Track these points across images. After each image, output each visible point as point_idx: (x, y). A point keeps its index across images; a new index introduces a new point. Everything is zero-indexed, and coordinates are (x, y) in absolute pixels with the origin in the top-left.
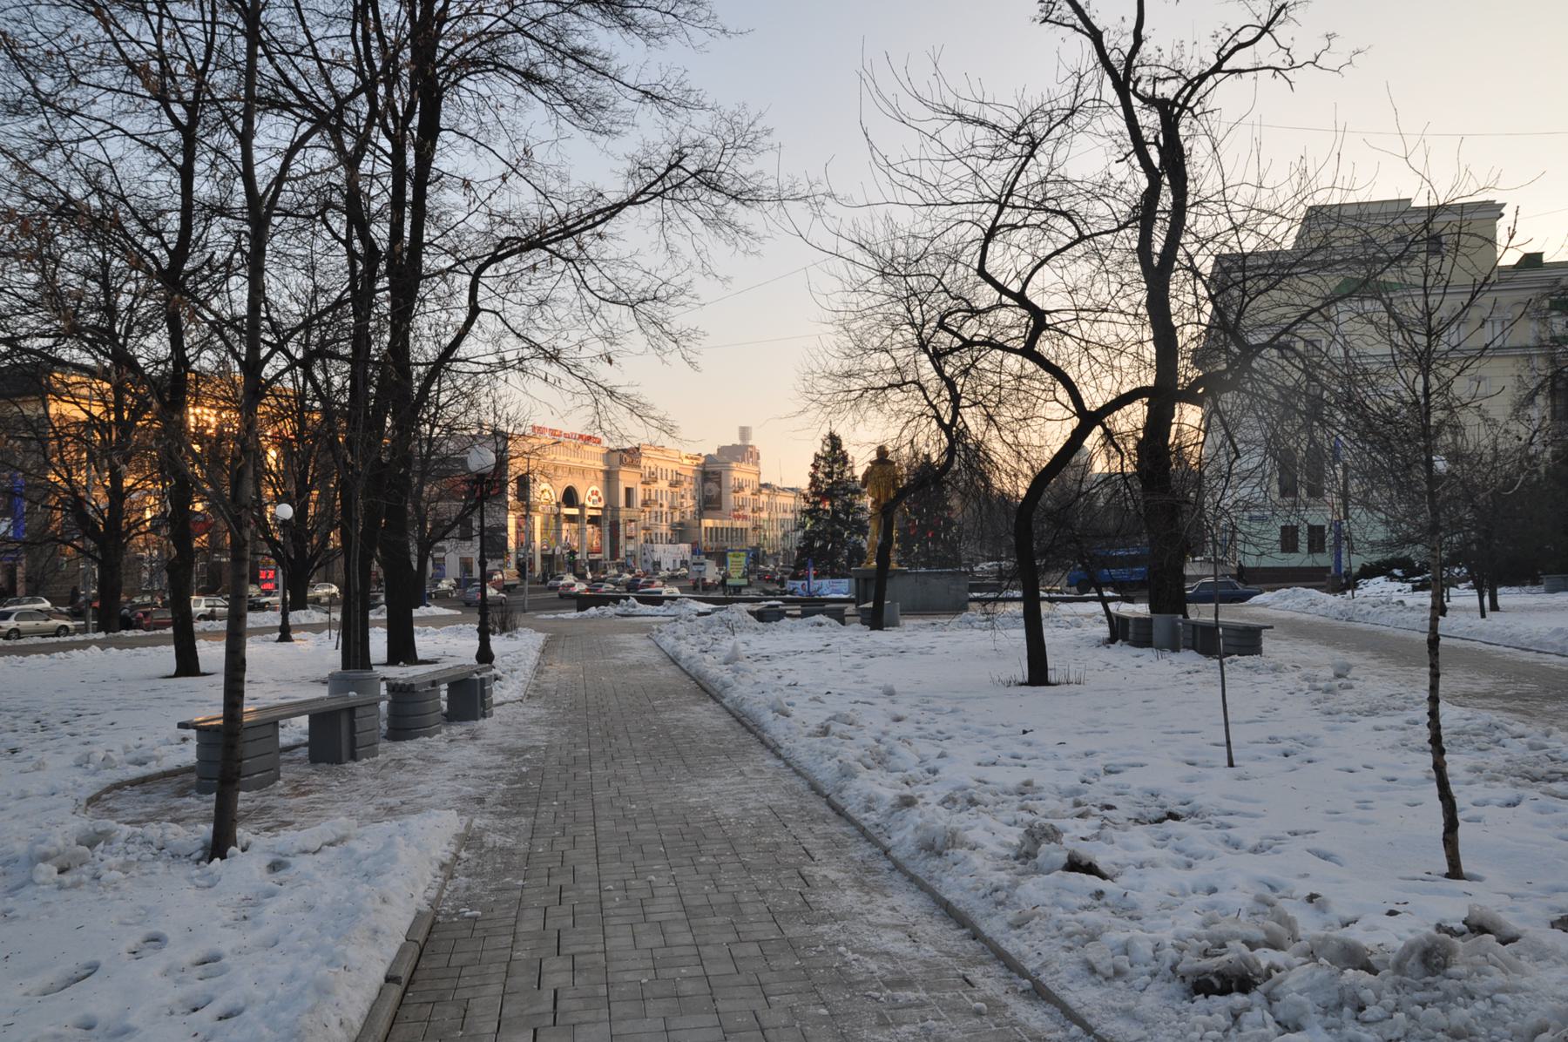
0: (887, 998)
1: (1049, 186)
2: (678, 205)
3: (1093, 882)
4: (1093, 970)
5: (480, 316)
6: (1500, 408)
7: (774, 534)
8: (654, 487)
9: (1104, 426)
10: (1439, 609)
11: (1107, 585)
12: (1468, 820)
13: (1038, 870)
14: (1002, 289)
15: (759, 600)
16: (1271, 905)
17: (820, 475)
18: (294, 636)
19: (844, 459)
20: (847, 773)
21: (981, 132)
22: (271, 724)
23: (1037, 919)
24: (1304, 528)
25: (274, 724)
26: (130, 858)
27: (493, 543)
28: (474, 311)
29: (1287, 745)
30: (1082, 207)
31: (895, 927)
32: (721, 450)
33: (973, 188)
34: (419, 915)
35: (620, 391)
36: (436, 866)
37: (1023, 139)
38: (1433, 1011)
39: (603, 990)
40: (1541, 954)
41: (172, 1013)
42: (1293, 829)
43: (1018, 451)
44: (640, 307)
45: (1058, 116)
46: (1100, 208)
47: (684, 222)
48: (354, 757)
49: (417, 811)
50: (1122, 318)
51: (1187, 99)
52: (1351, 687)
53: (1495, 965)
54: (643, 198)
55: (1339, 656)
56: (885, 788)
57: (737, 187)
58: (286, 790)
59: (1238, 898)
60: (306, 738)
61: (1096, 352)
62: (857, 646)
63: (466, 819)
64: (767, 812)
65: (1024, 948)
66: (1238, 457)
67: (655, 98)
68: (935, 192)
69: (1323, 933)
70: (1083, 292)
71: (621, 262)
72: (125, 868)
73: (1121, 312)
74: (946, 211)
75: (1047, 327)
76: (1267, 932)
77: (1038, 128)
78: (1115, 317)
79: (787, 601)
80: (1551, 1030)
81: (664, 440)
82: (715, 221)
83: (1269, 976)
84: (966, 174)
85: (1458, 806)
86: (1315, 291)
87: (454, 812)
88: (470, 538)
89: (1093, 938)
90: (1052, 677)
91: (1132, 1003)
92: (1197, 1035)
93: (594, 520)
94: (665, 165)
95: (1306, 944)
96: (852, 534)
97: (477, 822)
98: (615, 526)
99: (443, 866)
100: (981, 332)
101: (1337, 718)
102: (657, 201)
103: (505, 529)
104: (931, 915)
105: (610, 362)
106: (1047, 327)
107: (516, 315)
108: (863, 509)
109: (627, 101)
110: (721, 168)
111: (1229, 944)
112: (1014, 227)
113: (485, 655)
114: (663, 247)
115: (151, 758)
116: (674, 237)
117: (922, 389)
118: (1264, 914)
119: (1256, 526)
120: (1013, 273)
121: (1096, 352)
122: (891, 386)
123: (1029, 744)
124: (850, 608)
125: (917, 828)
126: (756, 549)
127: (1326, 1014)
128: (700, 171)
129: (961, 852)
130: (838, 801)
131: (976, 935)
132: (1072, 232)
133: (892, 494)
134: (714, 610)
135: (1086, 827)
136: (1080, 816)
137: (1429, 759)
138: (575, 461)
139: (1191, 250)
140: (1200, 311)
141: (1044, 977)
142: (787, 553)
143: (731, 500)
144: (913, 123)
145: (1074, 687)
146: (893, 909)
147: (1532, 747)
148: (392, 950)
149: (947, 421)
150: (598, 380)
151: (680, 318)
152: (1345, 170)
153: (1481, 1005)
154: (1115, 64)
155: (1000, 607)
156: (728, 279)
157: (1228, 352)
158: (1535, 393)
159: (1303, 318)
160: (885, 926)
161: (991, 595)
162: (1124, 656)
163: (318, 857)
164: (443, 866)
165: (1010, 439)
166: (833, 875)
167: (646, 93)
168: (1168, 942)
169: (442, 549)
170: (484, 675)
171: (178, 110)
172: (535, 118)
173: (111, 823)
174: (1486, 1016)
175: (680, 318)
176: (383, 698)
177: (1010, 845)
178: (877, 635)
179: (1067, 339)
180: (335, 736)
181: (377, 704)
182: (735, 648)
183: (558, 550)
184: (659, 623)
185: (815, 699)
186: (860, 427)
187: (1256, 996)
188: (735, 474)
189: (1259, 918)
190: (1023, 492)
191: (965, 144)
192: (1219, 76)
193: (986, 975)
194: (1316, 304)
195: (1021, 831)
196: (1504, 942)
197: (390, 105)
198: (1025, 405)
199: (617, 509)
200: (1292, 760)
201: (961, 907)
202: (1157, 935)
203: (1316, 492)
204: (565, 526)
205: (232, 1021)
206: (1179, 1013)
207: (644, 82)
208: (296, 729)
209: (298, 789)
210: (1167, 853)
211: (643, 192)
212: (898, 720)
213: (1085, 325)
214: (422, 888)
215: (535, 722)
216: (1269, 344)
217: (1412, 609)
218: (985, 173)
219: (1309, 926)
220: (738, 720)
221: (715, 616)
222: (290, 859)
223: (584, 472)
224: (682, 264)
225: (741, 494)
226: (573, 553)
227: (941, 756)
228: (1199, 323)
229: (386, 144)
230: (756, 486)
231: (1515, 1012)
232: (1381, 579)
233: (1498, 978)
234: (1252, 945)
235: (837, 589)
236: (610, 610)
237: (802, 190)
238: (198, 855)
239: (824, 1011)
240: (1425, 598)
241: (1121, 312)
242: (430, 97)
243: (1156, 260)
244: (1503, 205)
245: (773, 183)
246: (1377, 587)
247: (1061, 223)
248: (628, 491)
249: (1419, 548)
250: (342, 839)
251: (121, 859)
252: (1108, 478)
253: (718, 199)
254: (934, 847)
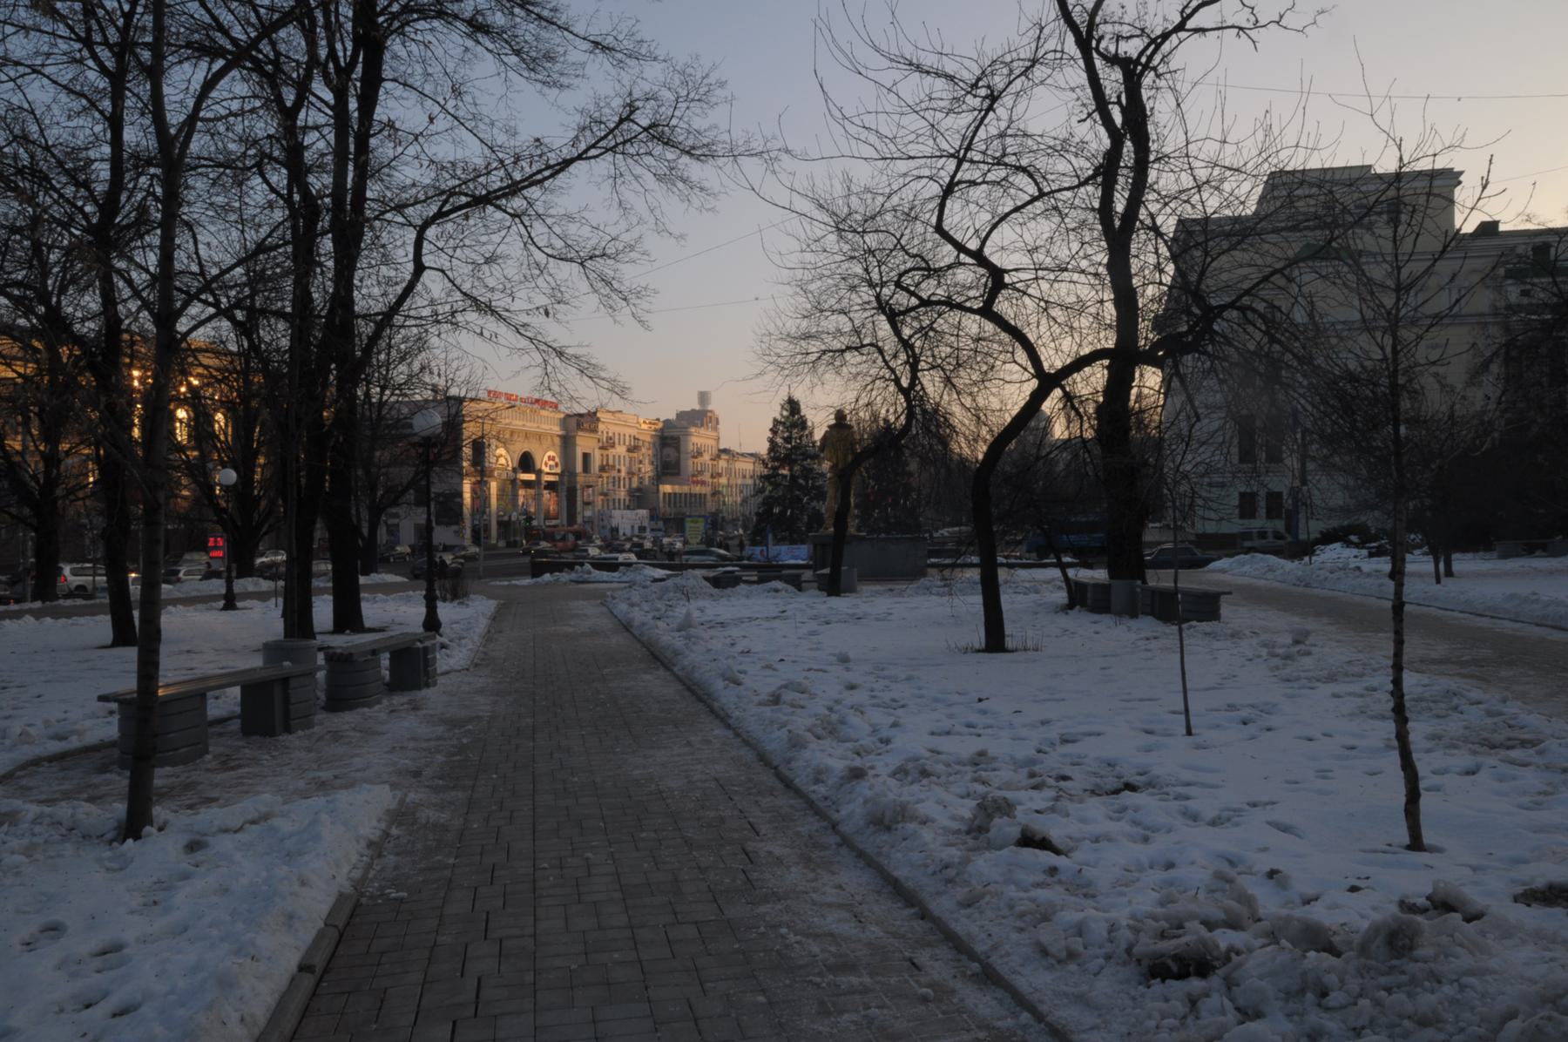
0: (829, 984)
1: (1009, 141)
2: (629, 161)
3: (1047, 858)
4: (1044, 952)
5: (426, 273)
6: (1456, 374)
7: (733, 499)
8: (612, 452)
9: (1063, 388)
10: (1397, 574)
11: (1066, 551)
12: (1428, 790)
13: (991, 846)
14: (960, 248)
15: (715, 566)
16: (1230, 881)
17: (779, 440)
18: (239, 604)
19: (802, 424)
20: (796, 744)
21: (940, 83)
22: (196, 696)
23: (988, 898)
24: (1262, 493)
25: (202, 696)
26: (35, 840)
27: (449, 509)
28: (419, 268)
29: (1244, 713)
30: (1042, 163)
31: (840, 906)
32: (681, 415)
33: (931, 142)
34: (342, 897)
35: (570, 351)
36: (363, 843)
37: (983, 92)
38: (1400, 996)
39: (529, 978)
40: (1507, 932)
41: (62, 1011)
43: (978, 415)
44: (588, 264)
45: (1018, 67)
46: (1062, 166)
47: (636, 178)
48: (288, 730)
49: (350, 785)
50: (1082, 278)
51: (1150, 58)
52: (1309, 654)
53: (1461, 945)
54: (593, 152)
55: (1297, 621)
56: (835, 759)
57: (690, 142)
58: (214, 764)
59: (1196, 874)
60: (238, 710)
61: (1056, 312)
62: (814, 612)
63: (399, 794)
64: (713, 785)
65: (974, 929)
66: (1198, 419)
67: (606, 49)
68: (891, 146)
69: (1284, 912)
70: (1042, 250)
71: (570, 218)
72: (28, 851)
73: (1083, 272)
74: (902, 166)
75: (1006, 286)
76: (1226, 911)
77: (999, 81)
78: (1076, 276)
79: (744, 567)
80: (1521, 1017)
81: (616, 403)
82: (669, 177)
83: (1229, 959)
84: (925, 127)
85: (1420, 774)
86: (1278, 253)
87: (387, 787)
89: (1046, 918)
90: (1009, 643)
91: (1085, 988)
92: (1152, 1023)
93: (551, 486)
94: (616, 119)
95: (1266, 925)
96: (811, 499)
97: (412, 796)
99: (371, 844)
100: (939, 291)
101: (1295, 685)
102: (609, 156)
103: (460, 495)
104: (879, 893)
105: (547, 314)
106: (1006, 286)
107: (461, 271)
108: (823, 475)
109: (577, 53)
110: (674, 122)
111: (1187, 925)
112: (973, 183)
113: (432, 623)
114: (615, 204)
115: (73, 732)
116: (627, 195)
117: (881, 351)
118: (1224, 891)
119: (1216, 492)
120: (972, 230)
121: (1056, 312)
122: (849, 348)
123: (984, 712)
124: (807, 575)
125: (866, 802)
126: (715, 515)
127: (1287, 1000)
128: (651, 127)
129: (911, 826)
130: (787, 773)
131: (924, 915)
132: (1032, 190)
133: (850, 458)
134: (669, 576)
135: (1040, 799)
136: (1035, 787)
137: (1390, 727)
138: (531, 426)
139: (1154, 207)
140: (1161, 271)
141: (994, 960)
142: (746, 519)
143: (690, 465)
144: (871, 74)
145: (1031, 654)
146: (840, 887)
147: (1490, 714)
148: (307, 934)
149: (905, 383)
150: (549, 340)
151: (629, 274)
152: (1310, 126)
153: (1448, 990)
154: (1078, 20)
155: (958, 573)
156: (682, 236)
157: (1190, 313)
158: (1490, 361)
159: (1266, 279)
160: (830, 905)
161: (948, 561)
162: (1083, 624)
163: (239, 836)
164: (371, 844)
165: (968, 402)
166: (778, 851)
167: (596, 44)
168: (1124, 923)
169: (396, 516)
170: (427, 644)
171: (104, 54)
172: (486, 74)
173: (17, 803)
174: (1453, 1001)
175: (629, 274)
176: (320, 668)
177: (962, 819)
178: (835, 602)
179: (1026, 299)
180: (269, 707)
181: (311, 674)
182: (688, 615)
183: (514, 516)
184: (613, 590)
185: (768, 667)
186: (818, 389)
187: (1215, 981)
188: (694, 439)
189: (1218, 895)
190: (981, 457)
191: (922, 96)
192: (1182, 35)
193: (934, 958)
194: (1279, 265)
195: (974, 803)
196: (1469, 919)
197: (332, 54)
198: (984, 368)
199: (573, 475)
200: (1252, 729)
201: (910, 884)
202: (1113, 914)
203: (1275, 458)
204: (521, 492)
205: (126, 1018)
206: (1134, 999)
207: (595, 31)
208: (228, 701)
209: (226, 764)
210: (1124, 826)
211: (593, 146)
212: (852, 687)
213: (1045, 285)
214: (345, 869)
215: (480, 691)
216: (1232, 305)
217: (1369, 575)
218: (943, 126)
219: (1269, 903)
220: (689, 689)
221: (670, 583)
222: (208, 839)
223: (540, 437)
224: (634, 220)
225: (700, 460)
226: (529, 519)
227: (895, 725)
228: (1161, 283)
229: (328, 96)
230: (715, 452)
231: (1483, 996)
232: (1337, 545)
233: (1465, 960)
234: (1210, 925)
235: (795, 555)
236: (565, 576)
237: (757, 145)
238: (110, 836)
239: (761, 999)
240: (1384, 564)
241: (1083, 272)
242: (371, 44)
243: (1117, 223)
244: (1461, 173)
245: (726, 137)
246: (1334, 553)
247: (1022, 180)
248: (586, 456)
249: (1377, 513)
250: (266, 817)
251: (25, 841)
252: (1066, 444)
253: (670, 154)
254: (886, 820)
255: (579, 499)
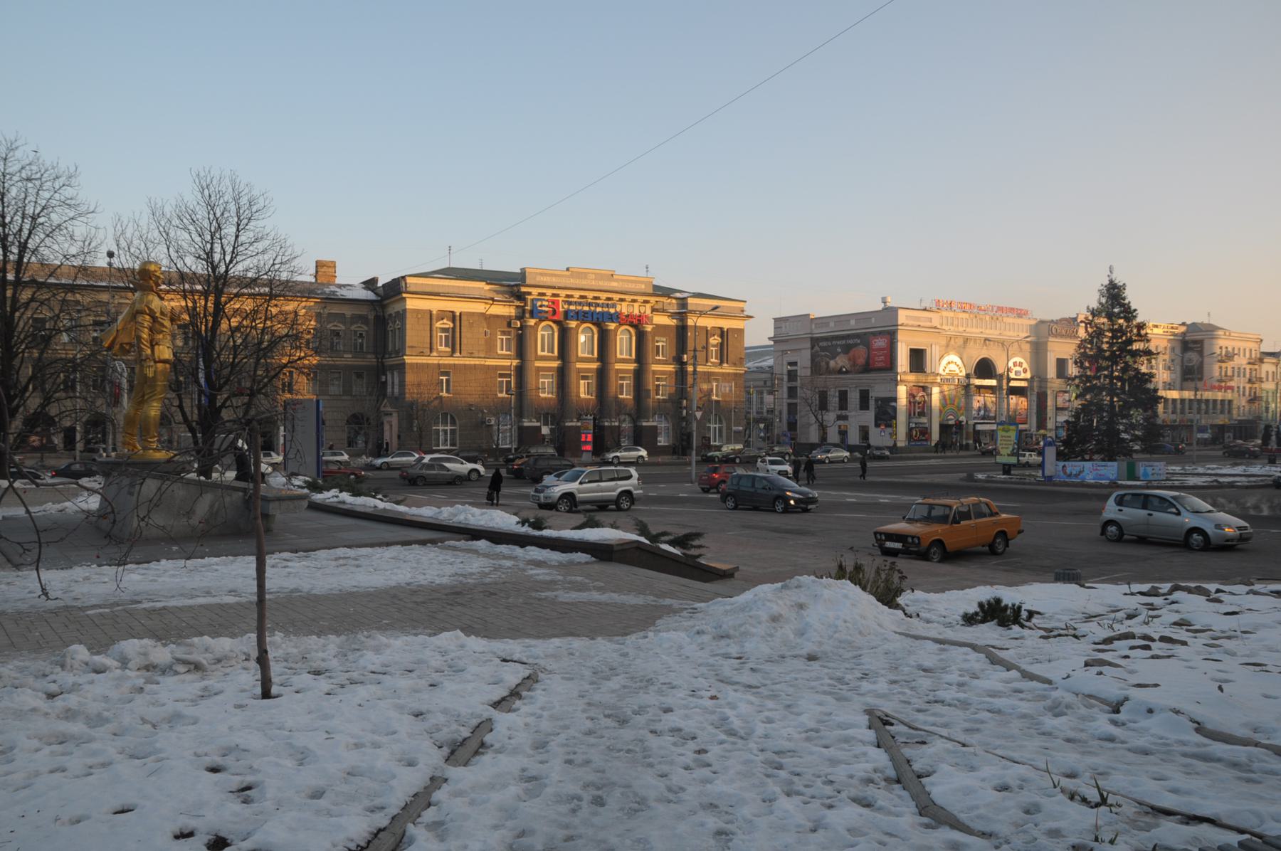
42: (118, 805)
88: (877, 400)
98: (1042, 398)
103: (895, 399)
143: (1215, 370)
255: (1050, 402)
